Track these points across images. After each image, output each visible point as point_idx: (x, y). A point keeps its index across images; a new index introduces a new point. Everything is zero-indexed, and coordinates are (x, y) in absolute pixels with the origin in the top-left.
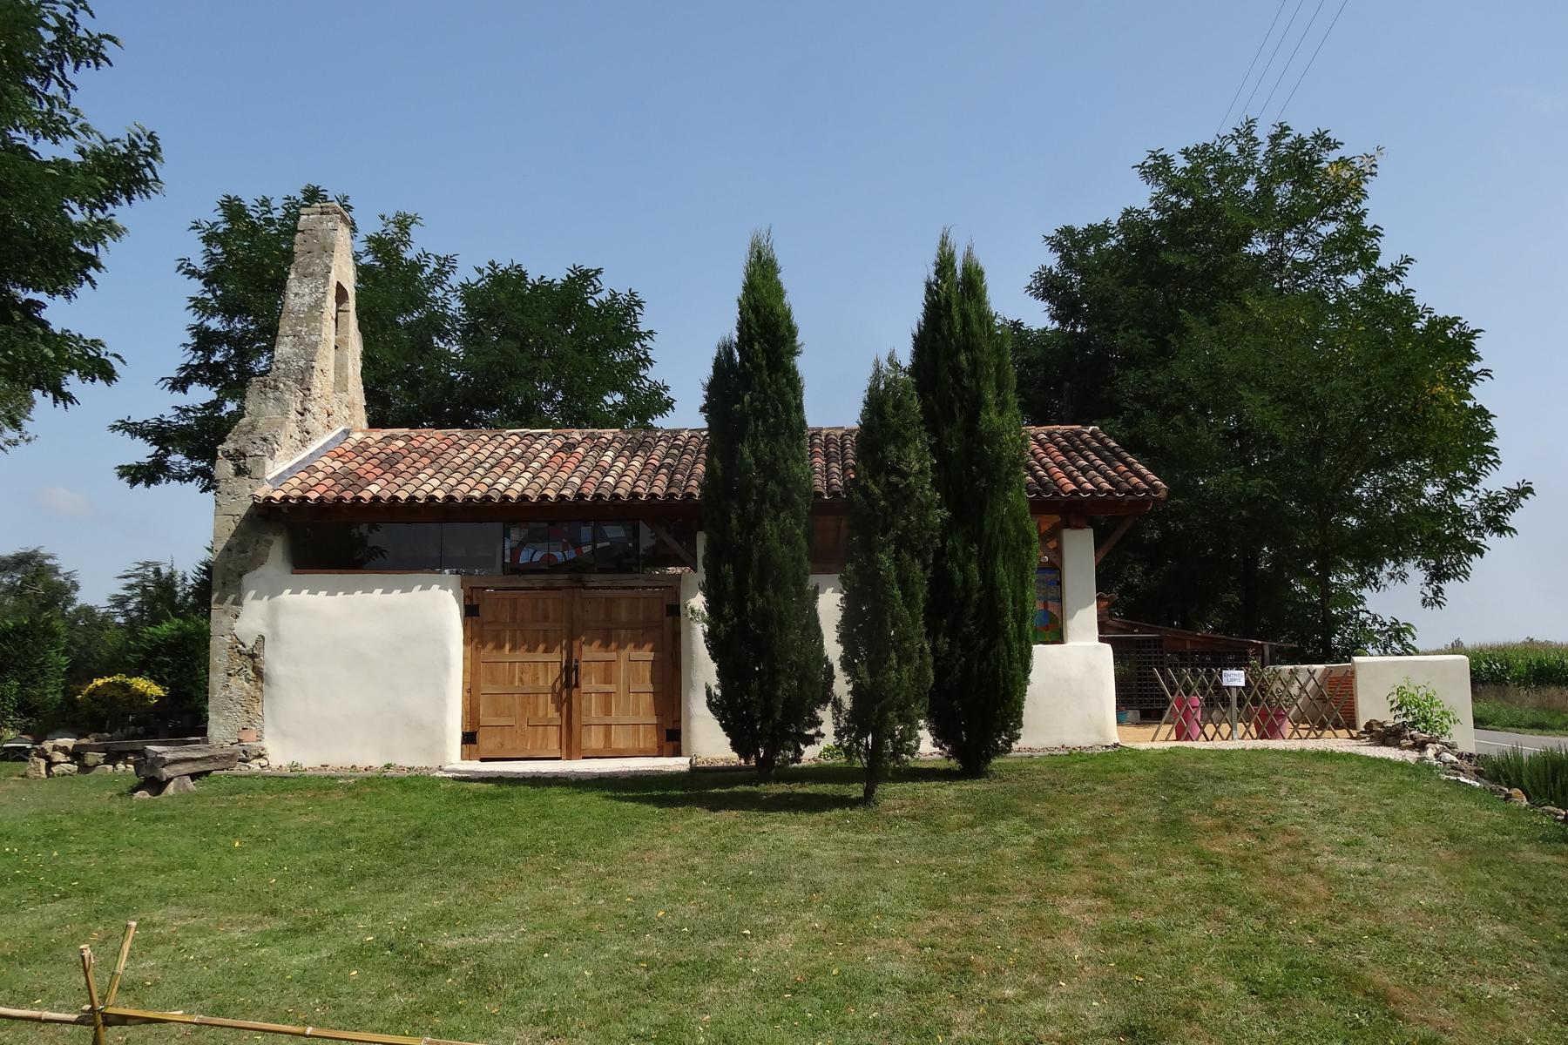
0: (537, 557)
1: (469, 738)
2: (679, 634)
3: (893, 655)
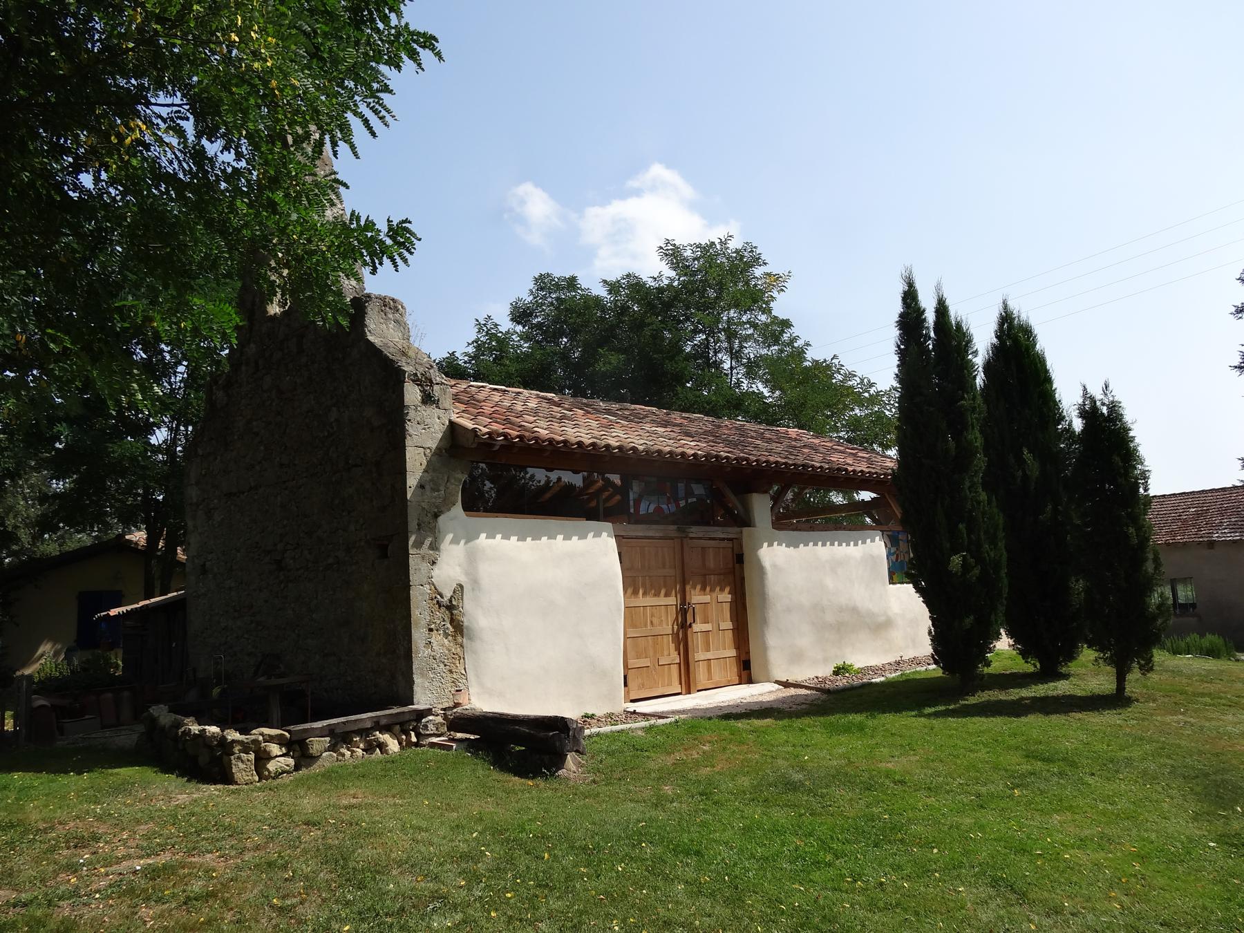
2: (743, 578)
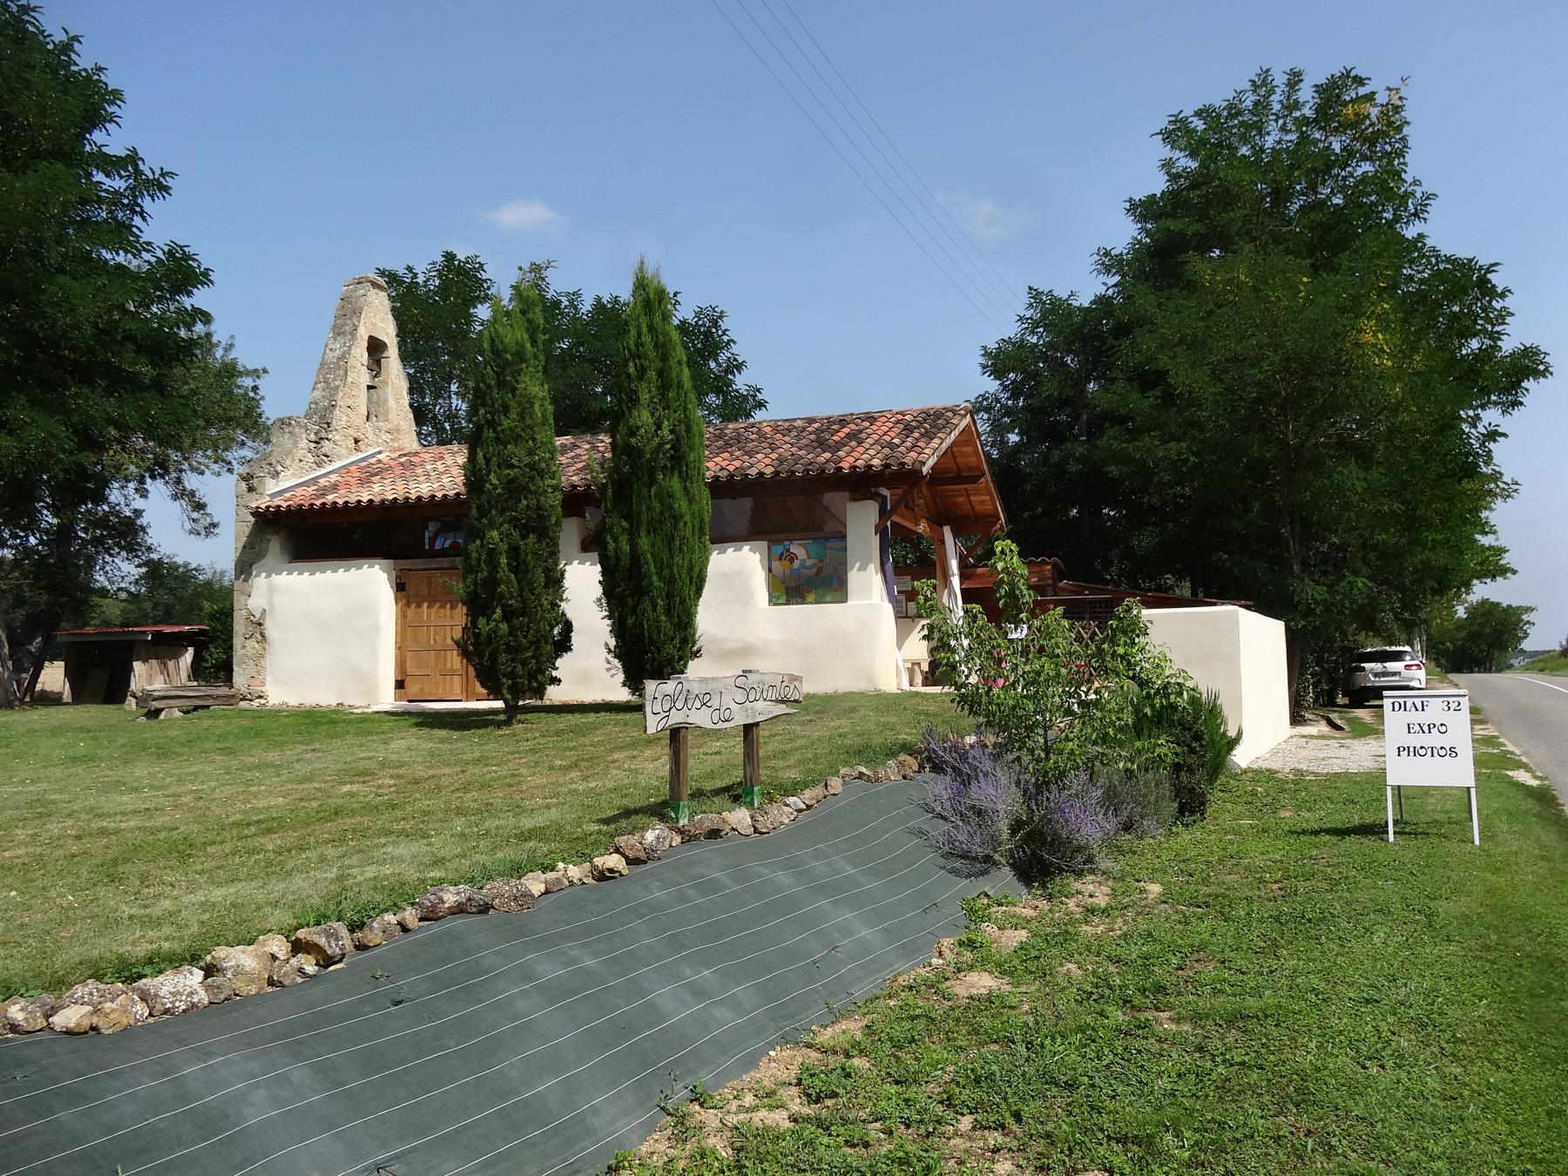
0: (447, 545)
1: (400, 685)
3: (499, 611)
